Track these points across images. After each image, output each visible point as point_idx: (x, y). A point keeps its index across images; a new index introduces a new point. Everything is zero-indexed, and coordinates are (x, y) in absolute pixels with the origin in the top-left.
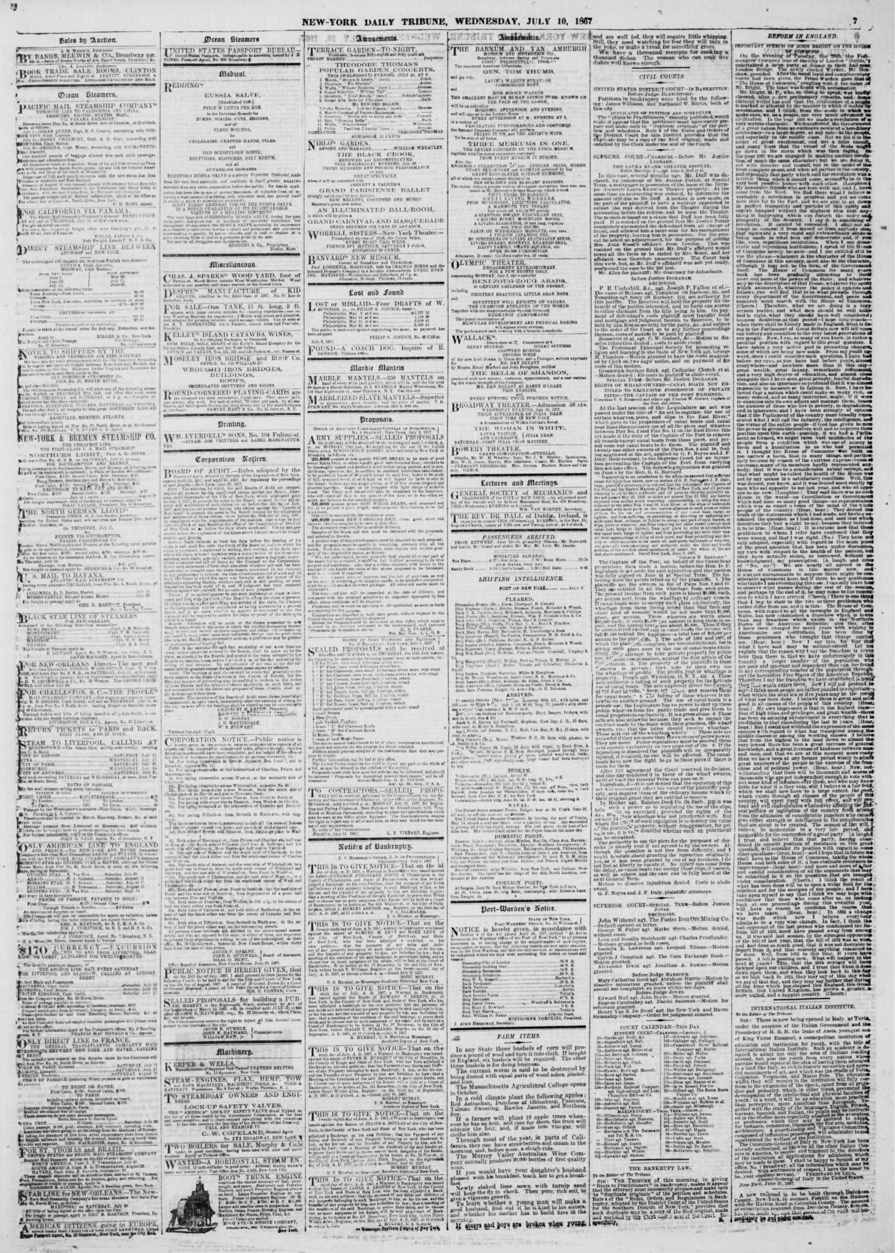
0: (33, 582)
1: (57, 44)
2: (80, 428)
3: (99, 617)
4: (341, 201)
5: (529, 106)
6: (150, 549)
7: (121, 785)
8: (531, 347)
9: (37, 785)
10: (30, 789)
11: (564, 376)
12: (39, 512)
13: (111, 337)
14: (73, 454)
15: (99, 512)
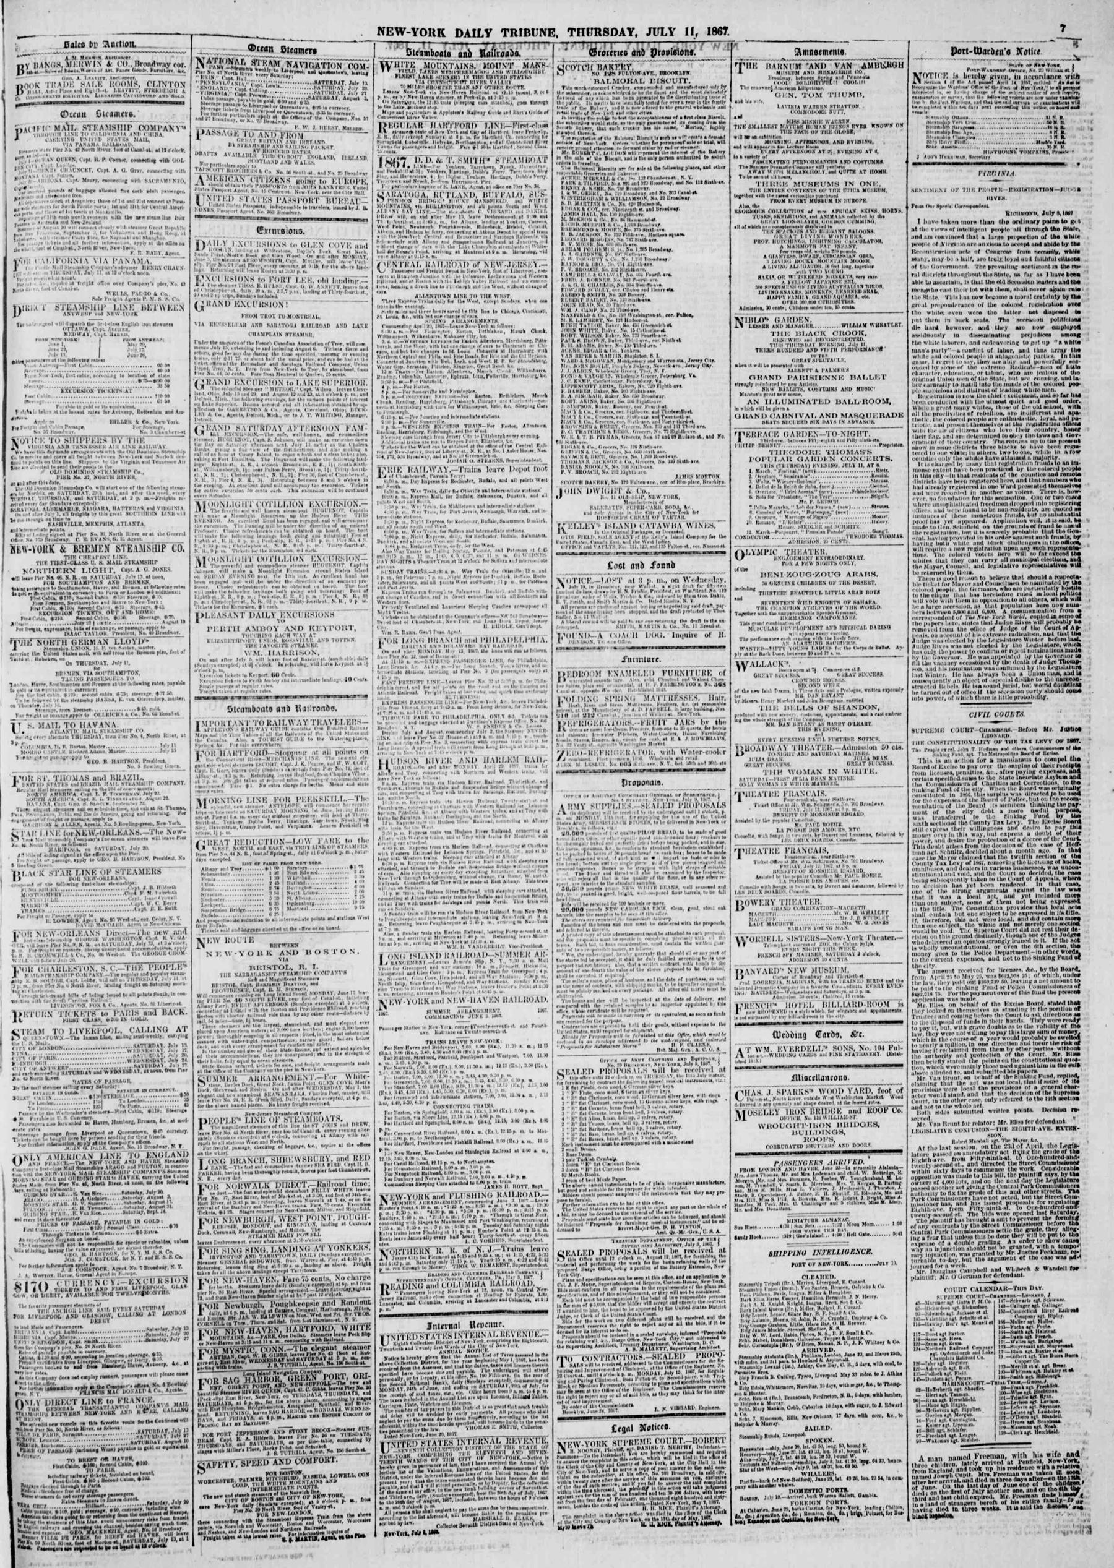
3: (112, 874)
7: (141, 1080)
8: (833, 675)
9: (34, 1084)
11: (874, 711)
12: (35, 642)
15: (111, 642)
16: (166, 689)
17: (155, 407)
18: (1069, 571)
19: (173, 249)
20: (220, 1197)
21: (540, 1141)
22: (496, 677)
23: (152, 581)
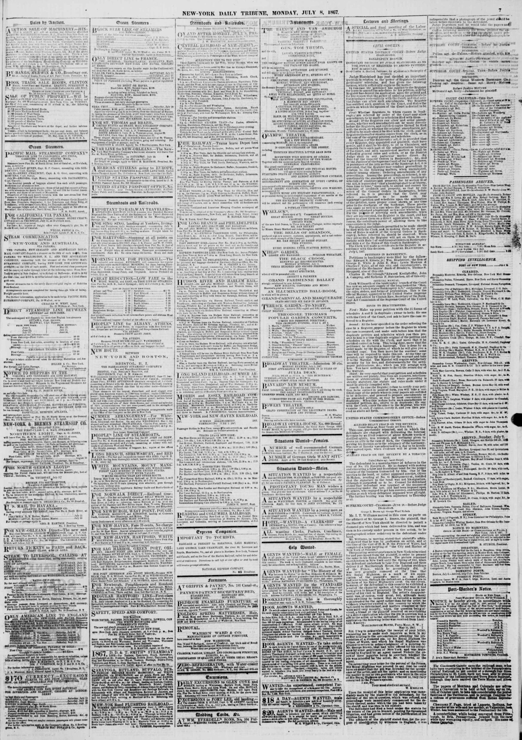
0: (13, 510)
2: (41, 418)
5: (308, 68)
6: (83, 490)
7: (66, 579)
10: (10, 583)
11: (328, 234)
12: (16, 467)
14: (37, 433)
15: (52, 467)
16: (78, 489)
17: (72, 356)
19: (81, 209)
20: (102, 500)
21: (254, 483)
22: (233, 241)
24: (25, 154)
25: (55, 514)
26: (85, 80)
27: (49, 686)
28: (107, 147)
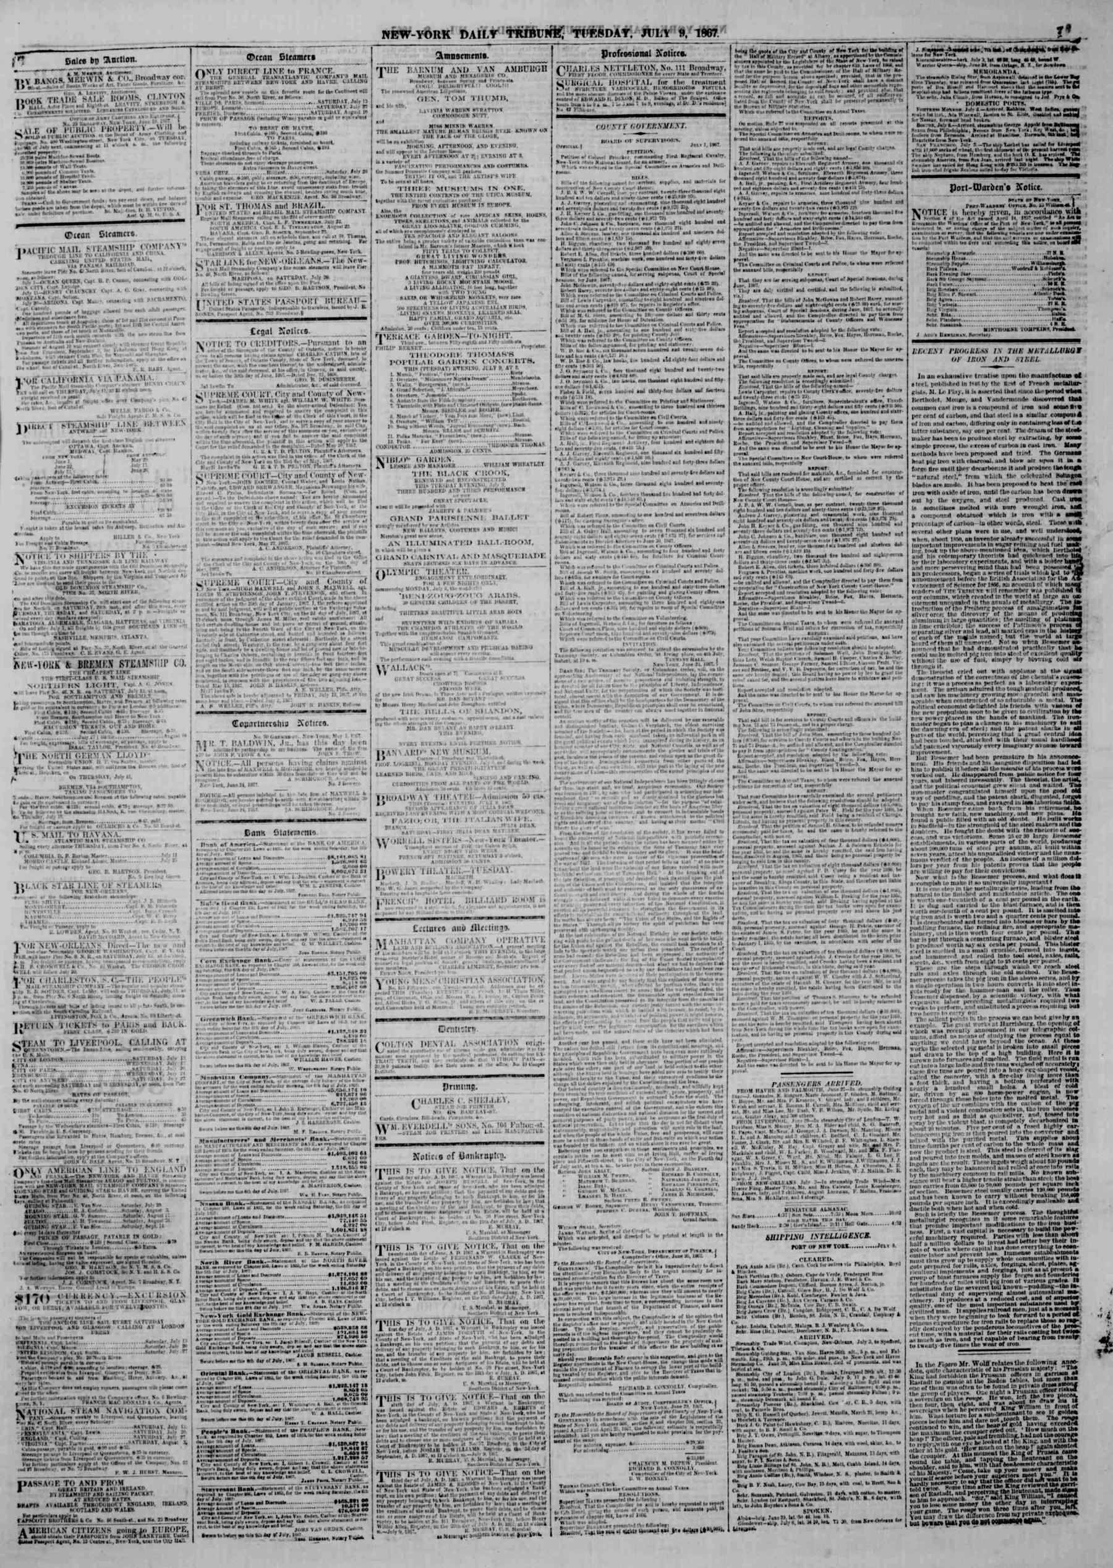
1: (63, 65)
4: (417, 533)
12: (39, 756)
13: (130, 537)
16: (166, 801)
18: (1069, 1012)
19: (173, 364)
23: (154, 696)
24: (58, 251)
25: (122, 852)
26: (179, 91)
27: (104, 1317)
28: (228, 258)
